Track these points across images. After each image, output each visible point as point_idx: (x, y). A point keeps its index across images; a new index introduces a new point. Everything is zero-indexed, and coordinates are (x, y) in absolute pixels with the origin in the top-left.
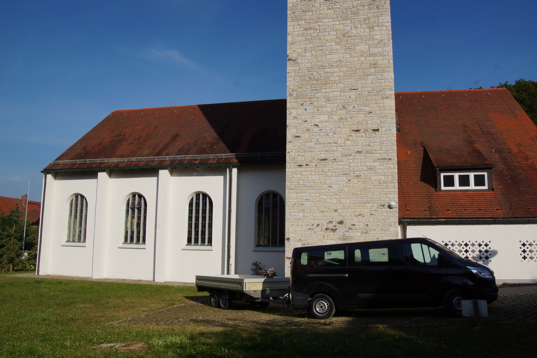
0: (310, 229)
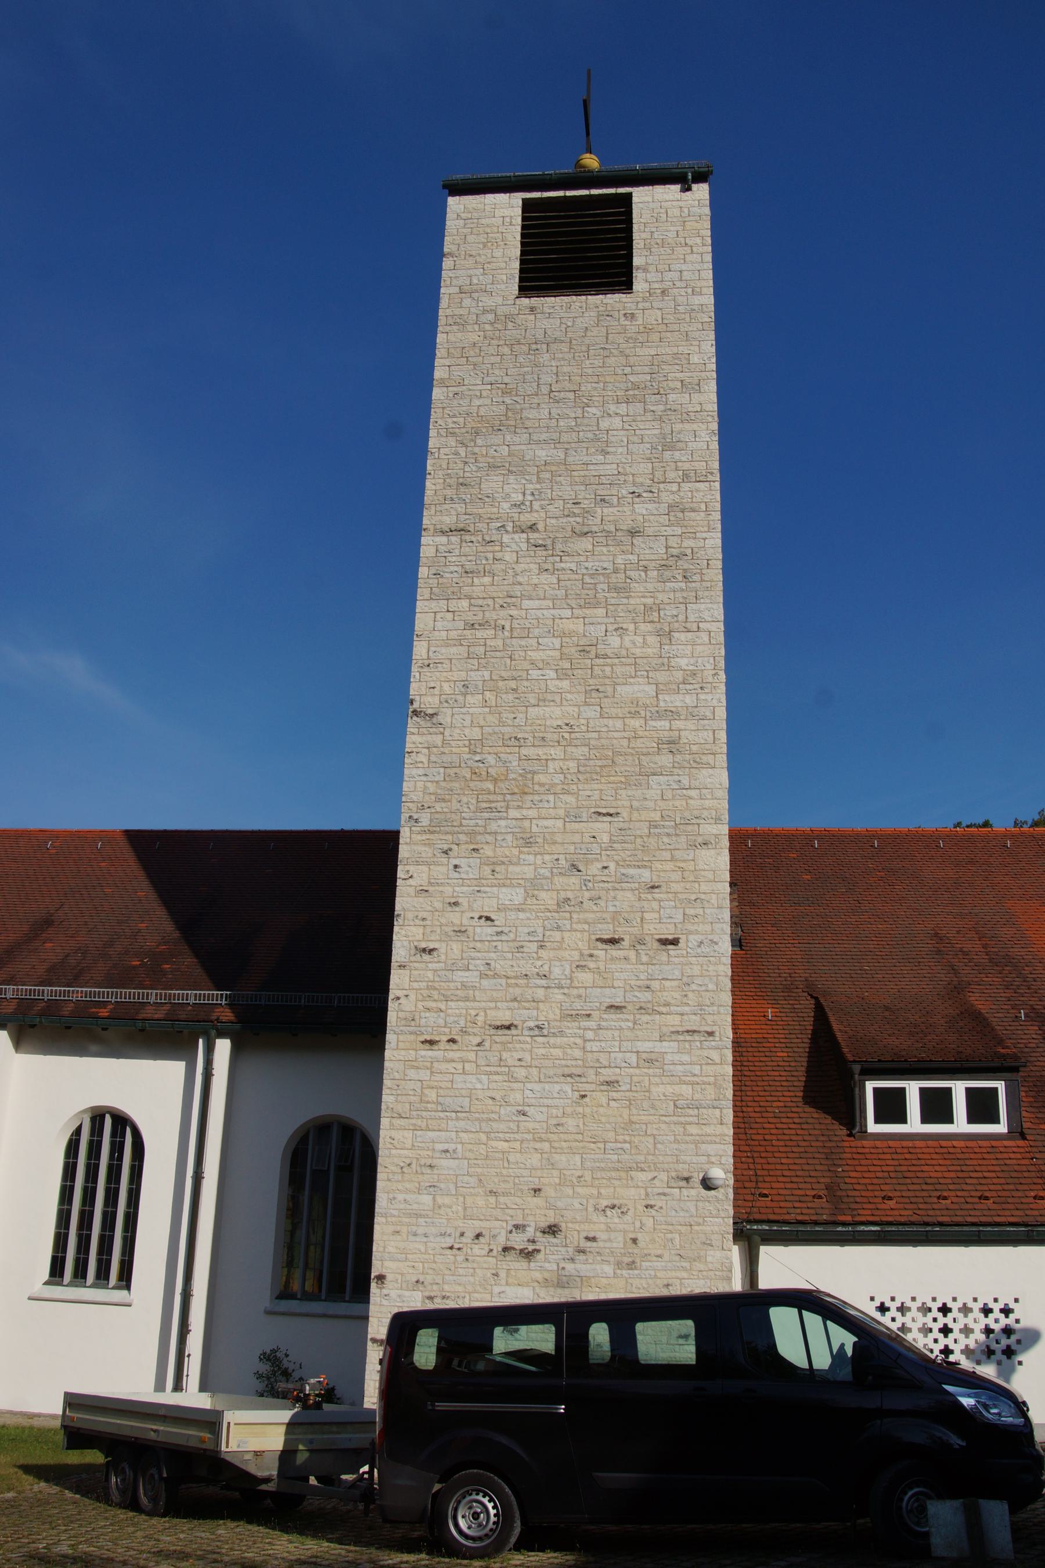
0: (451, 1248)
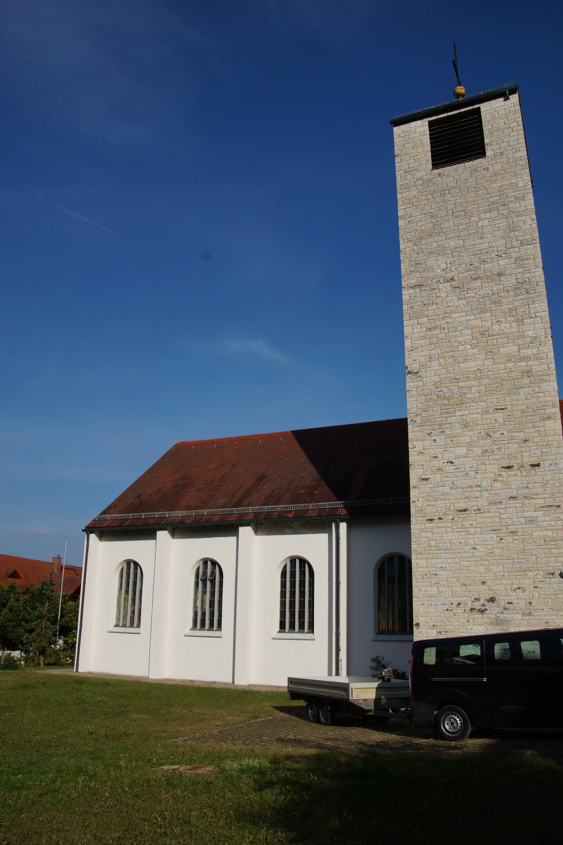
0: (447, 610)
